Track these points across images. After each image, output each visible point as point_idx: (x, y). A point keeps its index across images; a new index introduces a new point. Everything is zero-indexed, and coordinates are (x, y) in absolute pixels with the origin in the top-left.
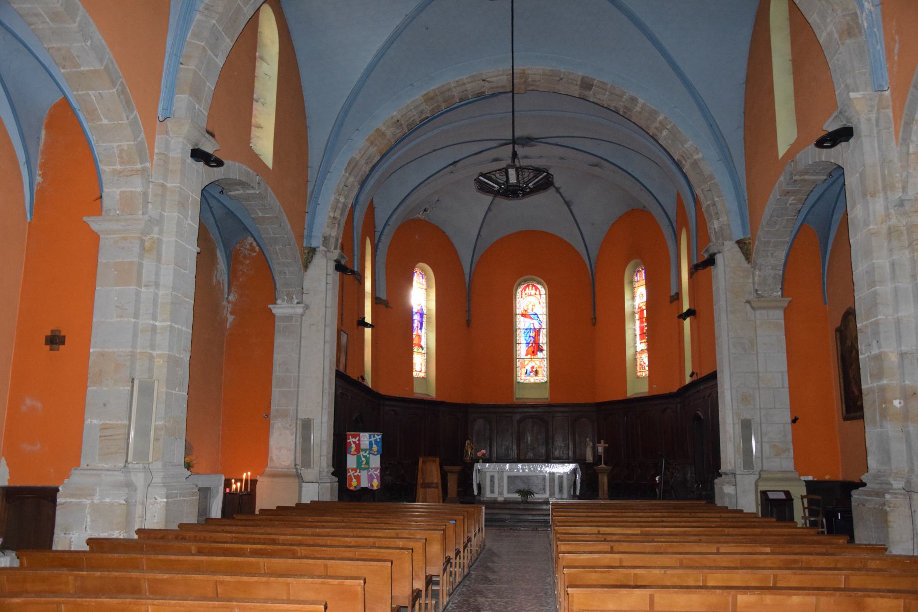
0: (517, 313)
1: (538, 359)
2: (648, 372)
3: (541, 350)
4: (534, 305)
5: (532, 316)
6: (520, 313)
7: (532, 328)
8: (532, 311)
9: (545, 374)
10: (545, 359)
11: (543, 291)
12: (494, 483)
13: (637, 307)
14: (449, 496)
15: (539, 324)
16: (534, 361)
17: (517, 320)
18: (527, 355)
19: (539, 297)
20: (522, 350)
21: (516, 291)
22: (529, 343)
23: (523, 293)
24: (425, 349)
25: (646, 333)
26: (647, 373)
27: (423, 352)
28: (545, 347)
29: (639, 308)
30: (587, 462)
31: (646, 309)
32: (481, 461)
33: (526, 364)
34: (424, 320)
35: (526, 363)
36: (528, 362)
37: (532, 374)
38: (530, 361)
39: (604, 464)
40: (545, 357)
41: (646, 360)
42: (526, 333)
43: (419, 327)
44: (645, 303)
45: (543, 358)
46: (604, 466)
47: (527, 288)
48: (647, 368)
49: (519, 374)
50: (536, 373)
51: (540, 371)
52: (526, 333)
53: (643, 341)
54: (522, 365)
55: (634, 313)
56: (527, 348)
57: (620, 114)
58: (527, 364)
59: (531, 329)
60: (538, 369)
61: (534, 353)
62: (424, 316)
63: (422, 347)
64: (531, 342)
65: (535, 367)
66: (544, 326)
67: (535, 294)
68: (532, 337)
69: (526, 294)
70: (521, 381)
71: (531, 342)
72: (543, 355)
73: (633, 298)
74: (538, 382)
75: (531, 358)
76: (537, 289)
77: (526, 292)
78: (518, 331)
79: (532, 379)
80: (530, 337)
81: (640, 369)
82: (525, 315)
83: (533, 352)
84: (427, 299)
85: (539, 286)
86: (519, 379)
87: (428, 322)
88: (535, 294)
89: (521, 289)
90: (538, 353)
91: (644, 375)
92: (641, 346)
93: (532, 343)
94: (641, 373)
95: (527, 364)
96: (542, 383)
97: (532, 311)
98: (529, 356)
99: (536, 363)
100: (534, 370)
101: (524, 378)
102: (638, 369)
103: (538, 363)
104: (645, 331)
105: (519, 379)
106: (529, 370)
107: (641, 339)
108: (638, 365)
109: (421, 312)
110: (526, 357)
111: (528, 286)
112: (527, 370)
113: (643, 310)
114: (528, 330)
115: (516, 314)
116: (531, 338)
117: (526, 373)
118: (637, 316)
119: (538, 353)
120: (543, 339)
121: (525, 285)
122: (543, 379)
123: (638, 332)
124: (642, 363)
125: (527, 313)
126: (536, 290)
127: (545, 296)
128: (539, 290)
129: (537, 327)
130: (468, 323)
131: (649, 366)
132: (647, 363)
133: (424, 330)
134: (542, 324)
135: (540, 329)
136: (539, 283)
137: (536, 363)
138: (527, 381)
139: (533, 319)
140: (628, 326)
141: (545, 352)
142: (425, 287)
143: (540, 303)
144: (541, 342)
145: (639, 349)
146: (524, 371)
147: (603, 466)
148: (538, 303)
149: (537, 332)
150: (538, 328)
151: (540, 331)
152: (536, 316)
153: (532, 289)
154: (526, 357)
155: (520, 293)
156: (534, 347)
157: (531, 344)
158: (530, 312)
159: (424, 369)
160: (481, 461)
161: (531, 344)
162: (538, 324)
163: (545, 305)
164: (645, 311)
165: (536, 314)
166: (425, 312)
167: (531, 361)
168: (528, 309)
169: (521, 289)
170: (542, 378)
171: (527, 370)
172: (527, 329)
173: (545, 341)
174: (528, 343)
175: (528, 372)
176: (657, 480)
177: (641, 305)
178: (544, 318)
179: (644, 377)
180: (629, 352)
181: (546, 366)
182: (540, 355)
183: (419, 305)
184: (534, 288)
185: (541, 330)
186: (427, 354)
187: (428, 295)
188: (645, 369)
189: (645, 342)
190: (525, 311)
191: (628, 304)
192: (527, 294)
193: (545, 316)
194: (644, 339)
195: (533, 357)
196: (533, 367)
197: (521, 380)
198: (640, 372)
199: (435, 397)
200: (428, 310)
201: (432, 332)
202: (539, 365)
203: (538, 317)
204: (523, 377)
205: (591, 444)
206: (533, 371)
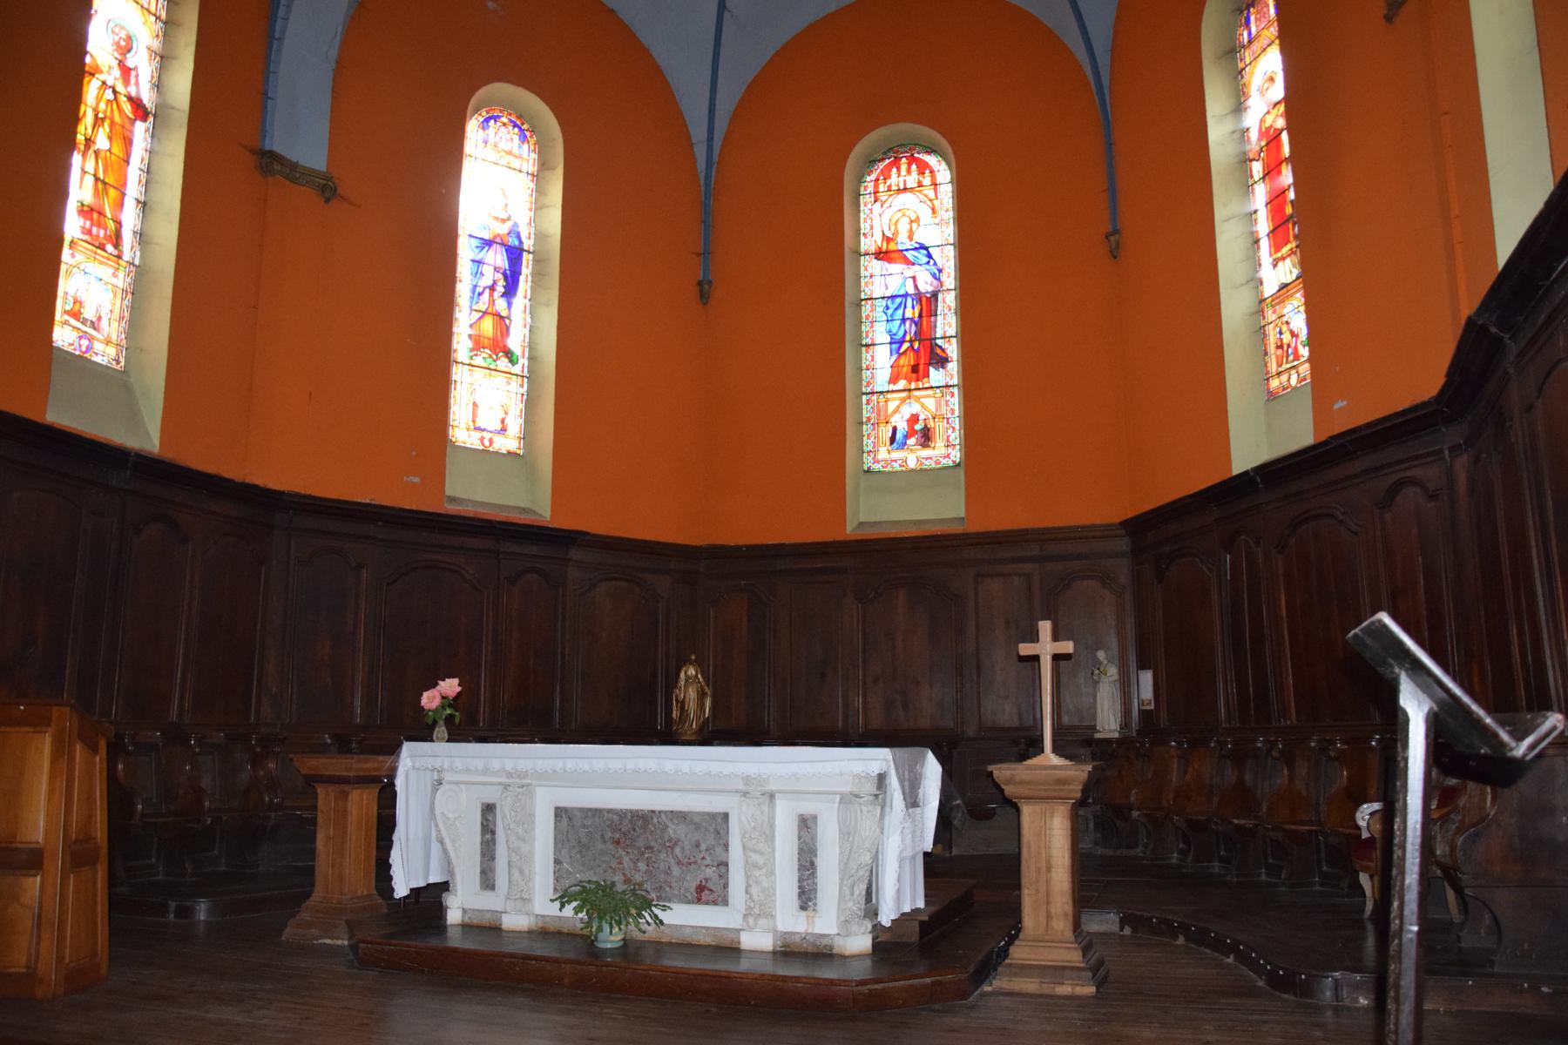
0: (863, 249)
1: (930, 392)
2: (1307, 366)
3: (942, 361)
4: (917, 220)
5: (909, 255)
6: (873, 249)
7: (911, 290)
8: (911, 239)
9: (955, 437)
10: (955, 390)
11: (944, 174)
12: (493, 841)
13: (1254, 135)
14: (317, 895)
15: (934, 276)
16: (918, 399)
17: (863, 273)
18: (893, 380)
19: (931, 194)
20: (880, 363)
21: (860, 180)
22: (901, 342)
23: (882, 188)
24: (524, 361)
25: (1291, 217)
26: (1305, 369)
27: (517, 369)
28: (952, 350)
29: (1264, 133)
30: (1098, 736)
31: (1290, 127)
32: (441, 730)
33: (890, 410)
34: (526, 270)
35: (892, 406)
36: (897, 403)
37: (911, 441)
38: (903, 400)
39: (1057, 750)
40: (955, 381)
41: (1299, 322)
42: (890, 312)
43: (500, 289)
44: (1282, 108)
45: (947, 386)
46: (1056, 760)
47: (894, 170)
48: (1304, 352)
49: (868, 444)
50: (926, 437)
51: (939, 428)
52: (890, 312)
53: (1285, 250)
54: (879, 415)
55: (1245, 161)
56: (895, 357)
57: (1495, 919)
58: (897, 410)
59: (906, 296)
60: (931, 424)
61: (917, 372)
62: (527, 259)
63: (509, 354)
64: (908, 338)
65: (922, 417)
66: (949, 280)
67: (920, 185)
68: (912, 319)
69: (889, 190)
70: (876, 467)
71: (908, 338)
72: (951, 374)
73: (1239, 108)
74: (933, 466)
75: (910, 390)
76: (923, 168)
77: (888, 182)
78: (866, 309)
79: (913, 457)
80: (904, 320)
81: (1279, 365)
82: (887, 252)
83: (915, 369)
84: (539, 206)
85: (932, 160)
86: (868, 461)
87: (538, 275)
88: (920, 185)
89: (873, 177)
90: (932, 370)
91: (1294, 381)
92: (1278, 272)
93: (911, 341)
94: (1284, 377)
95: (897, 410)
96: (947, 468)
97: (911, 239)
98: (902, 384)
99: (925, 405)
100: (918, 427)
101: (887, 456)
102: (1273, 368)
103: (930, 403)
104: (1289, 210)
105: (868, 461)
106: (902, 427)
107: (1276, 246)
108: (1272, 348)
109: (513, 241)
110: (892, 387)
111: (896, 163)
112: (895, 429)
113: (1279, 133)
114: (898, 300)
115: (858, 254)
116: (908, 323)
117: (893, 440)
118: (1257, 168)
119: (932, 370)
120: (946, 324)
121: (887, 161)
122: (948, 456)
123: (1263, 226)
124: (1286, 338)
125: (892, 246)
126: (921, 173)
127: (949, 188)
128: (932, 172)
129: (926, 285)
130: (704, 291)
131: (1312, 341)
132: (1303, 333)
133: (520, 300)
134: (944, 277)
135: (935, 295)
136: (930, 151)
137: (925, 405)
138: (896, 467)
139: (913, 264)
140: (1224, 208)
141: (953, 367)
142: (533, 169)
143: (934, 210)
144: (939, 335)
145: (1269, 289)
146: (886, 432)
147: (1050, 758)
148: (930, 211)
149: (928, 303)
150: (930, 289)
151: (937, 300)
152: (921, 256)
153: (909, 171)
154: (892, 387)
155: (871, 189)
156: (917, 352)
157: (906, 345)
158: (903, 242)
159: (515, 425)
160: (441, 730)
161: (906, 345)
162: (930, 279)
163: (951, 214)
164: (1285, 136)
165: (923, 247)
166: (528, 244)
167: (909, 398)
168: (896, 234)
169: (873, 177)
170: (943, 451)
171: (895, 429)
172: (893, 297)
173: (952, 331)
174: (897, 342)
175: (899, 436)
176: (1363, 824)
177: (1269, 120)
178: (947, 259)
179: (1295, 388)
180: (1234, 307)
181: (957, 413)
182: (936, 376)
183: (504, 221)
184: (914, 167)
185: (940, 297)
186: (532, 377)
187: (540, 191)
188: (1297, 357)
189: (1292, 252)
190: (889, 240)
191: (1218, 133)
192: (894, 188)
193: (950, 252)
194: (1288, 242)
195: (913, 386)
196: (914, 419)
197: (878, 462)
198: (1279, 374)
199: (548, 518)
200: (540, 237)
201: (547, 305)
202: (933, 409)
203: (929, 256)
204: (883, 454)
205: (1113, 671)
206: (916, 432)
